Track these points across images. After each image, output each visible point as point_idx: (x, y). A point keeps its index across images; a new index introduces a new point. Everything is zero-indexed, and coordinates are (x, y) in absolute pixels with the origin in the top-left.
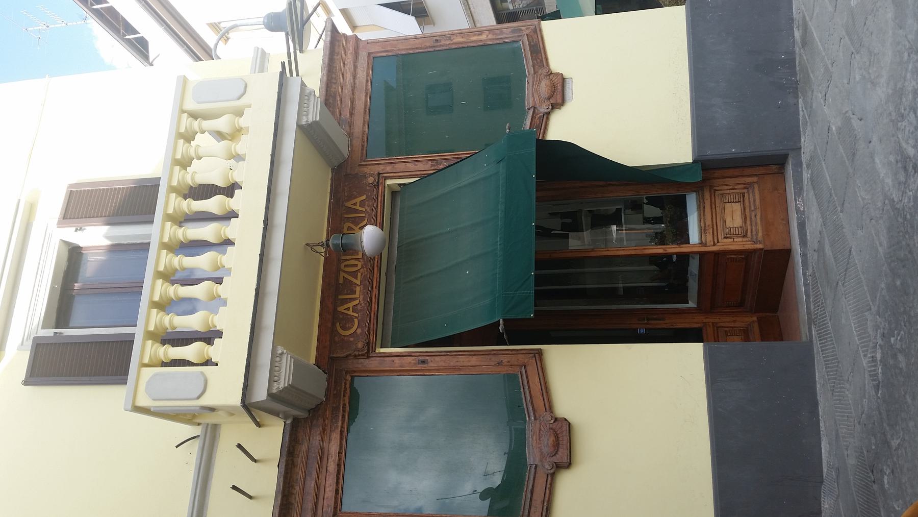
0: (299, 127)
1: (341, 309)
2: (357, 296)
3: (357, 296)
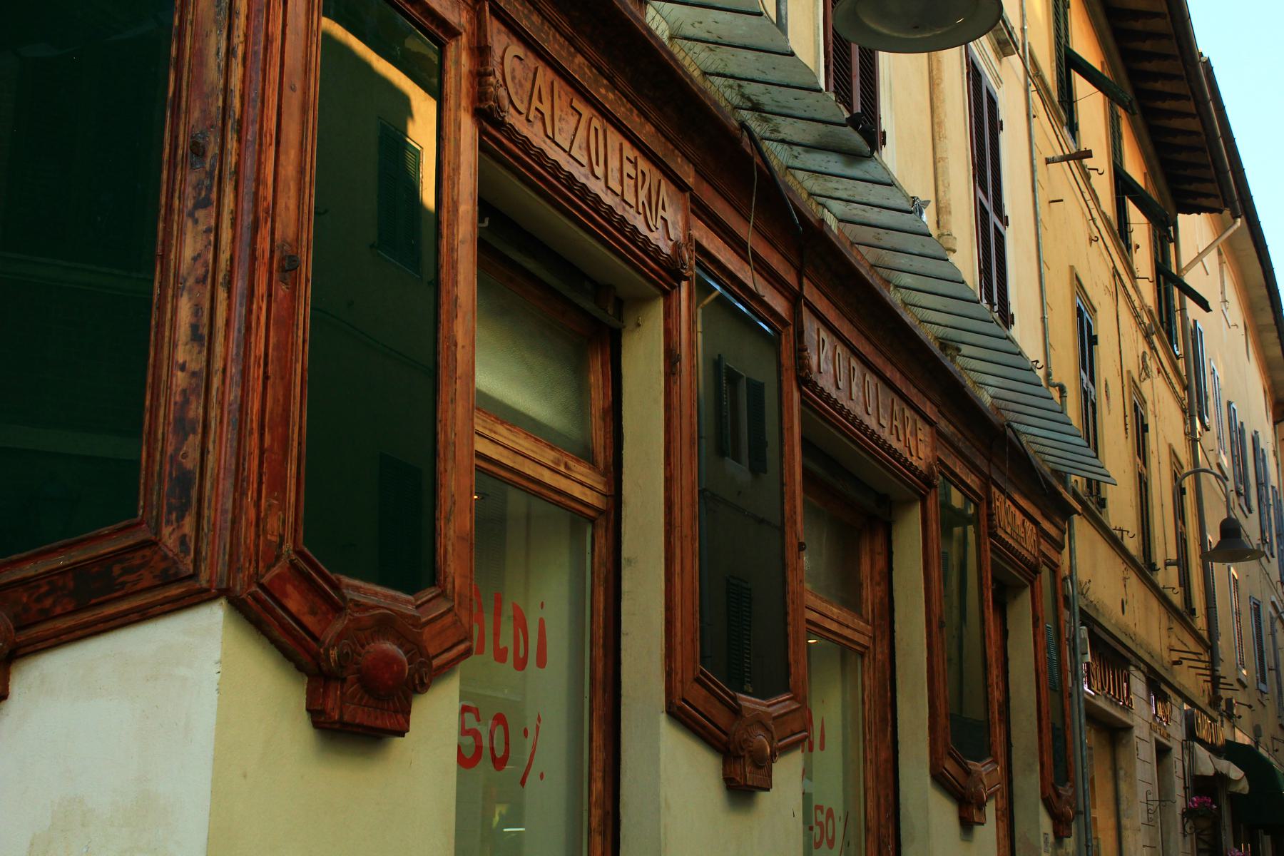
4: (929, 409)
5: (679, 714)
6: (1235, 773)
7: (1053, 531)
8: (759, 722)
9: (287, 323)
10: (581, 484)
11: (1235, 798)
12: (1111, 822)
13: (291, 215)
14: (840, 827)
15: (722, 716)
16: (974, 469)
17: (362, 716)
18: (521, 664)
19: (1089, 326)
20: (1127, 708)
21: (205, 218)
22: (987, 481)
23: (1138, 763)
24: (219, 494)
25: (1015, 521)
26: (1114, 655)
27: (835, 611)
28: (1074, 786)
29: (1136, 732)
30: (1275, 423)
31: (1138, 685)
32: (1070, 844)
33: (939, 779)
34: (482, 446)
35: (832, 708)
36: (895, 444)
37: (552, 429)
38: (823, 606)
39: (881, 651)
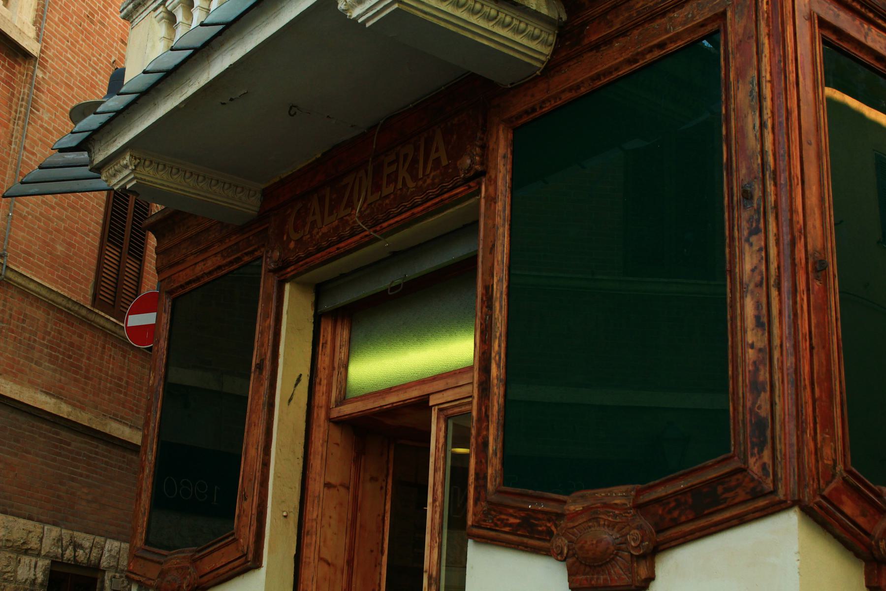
13: (818, 232)
21: (757, 241)
24: (786, 434)
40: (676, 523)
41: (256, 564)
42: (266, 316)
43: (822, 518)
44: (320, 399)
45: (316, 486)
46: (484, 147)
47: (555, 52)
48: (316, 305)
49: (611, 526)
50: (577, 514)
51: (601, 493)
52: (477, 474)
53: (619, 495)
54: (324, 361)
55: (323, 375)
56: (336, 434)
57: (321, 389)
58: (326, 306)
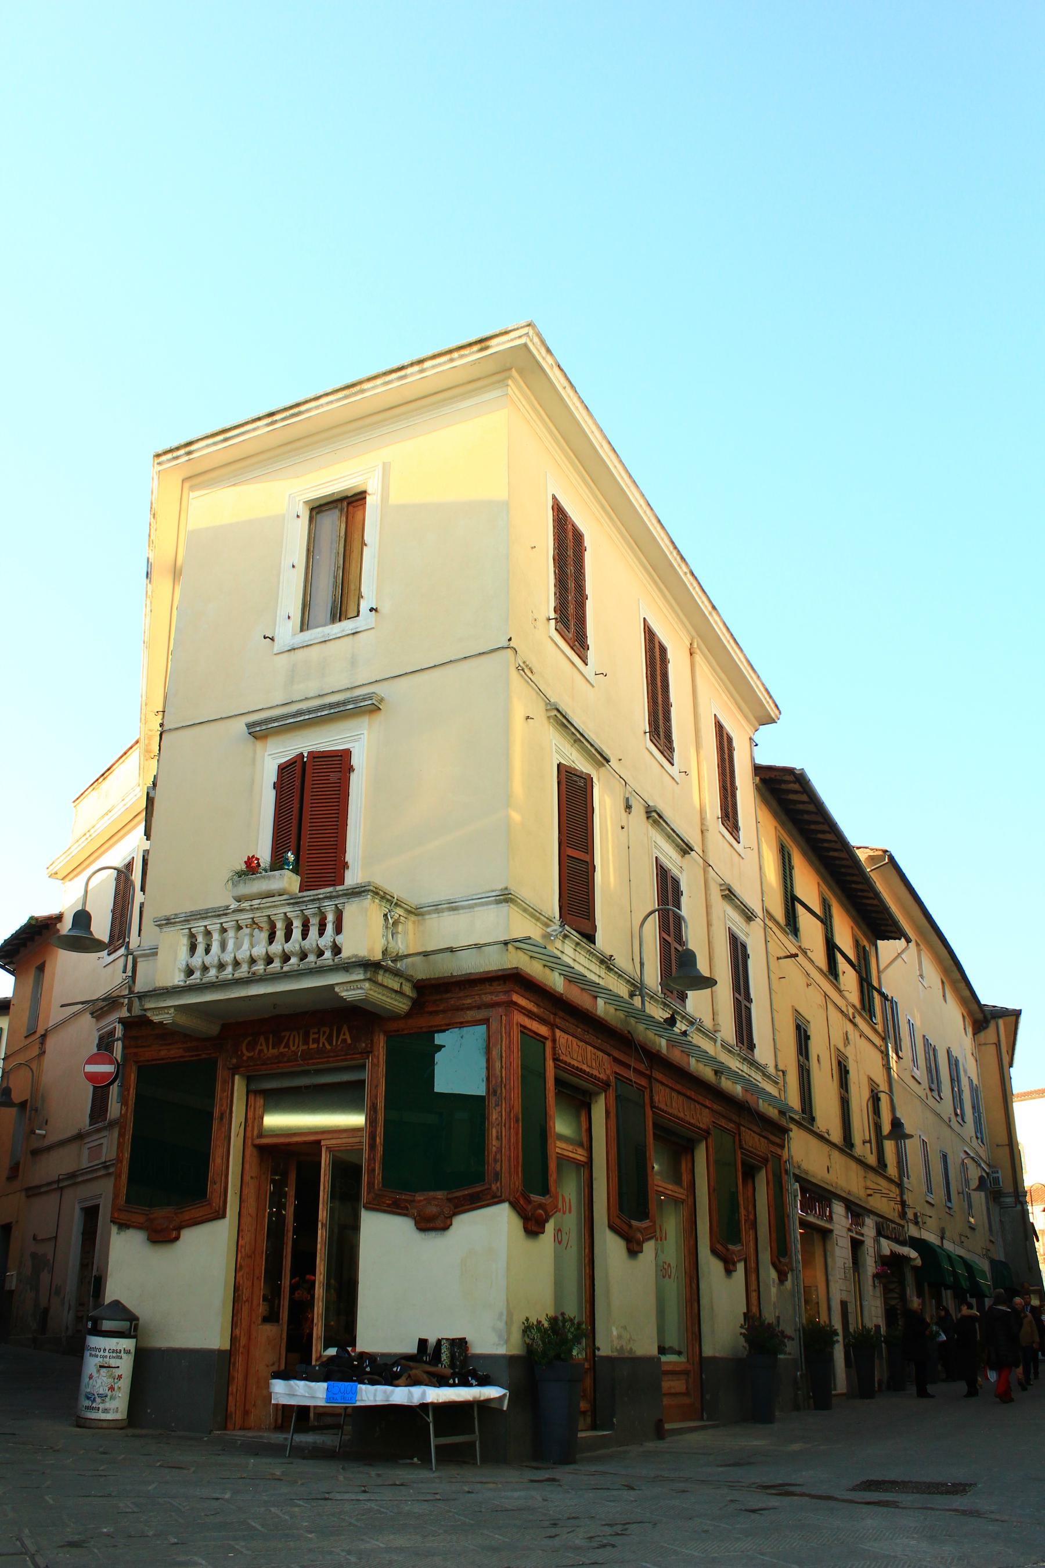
0: (332, 986)
1: (262, 1039)
2: (271, 1051)
3: (271, 1051)
4: (707, 1103)
5: (611, 1227)
6: (913, 1254)
7: (778, 1141)
8: (638, 1229)
9: (517, 1134)
10: (580, 1155)
11: (915, 1268)
12: (823, 1279)
13: (518, 1108)
14: (674, 1271)
15: (625, 1228)
16: (731, 1121)
17: (534, 1228)
18: (564, 1213)
19: (805, 1031)
20: (830, 1219)
21: (498, 1109)
22: (739, 1126)
23: (837, 1249)
24: (505, 1176)
25: (754, 1141)
26: (817, 1195)
27: (670, 1187)
28: (790, 1258)
29: (835, 1232)
30: (974, 1034)
31: (839, 1209)
32: (788, 1284)
33: (714, 1252)
34: (558, 1150)
35: (671, 1225)
36: (692, 1121)
37: (721, 1359)
38: (664, 1185)
39: (690, 1201)
40: (463, 1205)
41: (224, 1216)
42: (223, 1091)
43: (515, 1206)
44: (249, 1134)
45: (247, 1178)
46: (372, 1041)
47: (411, 1009)
48: (247, 1086)
49: (437, 1206)
50: (420, 1201)
51: (432, 1194)
52: (368, 1183)
53: (439, 1194)
54: (250, 1115)
55: (250, 1122)
56: (255, 1151)
57: (249, 1129)
58: (253, 1087)
